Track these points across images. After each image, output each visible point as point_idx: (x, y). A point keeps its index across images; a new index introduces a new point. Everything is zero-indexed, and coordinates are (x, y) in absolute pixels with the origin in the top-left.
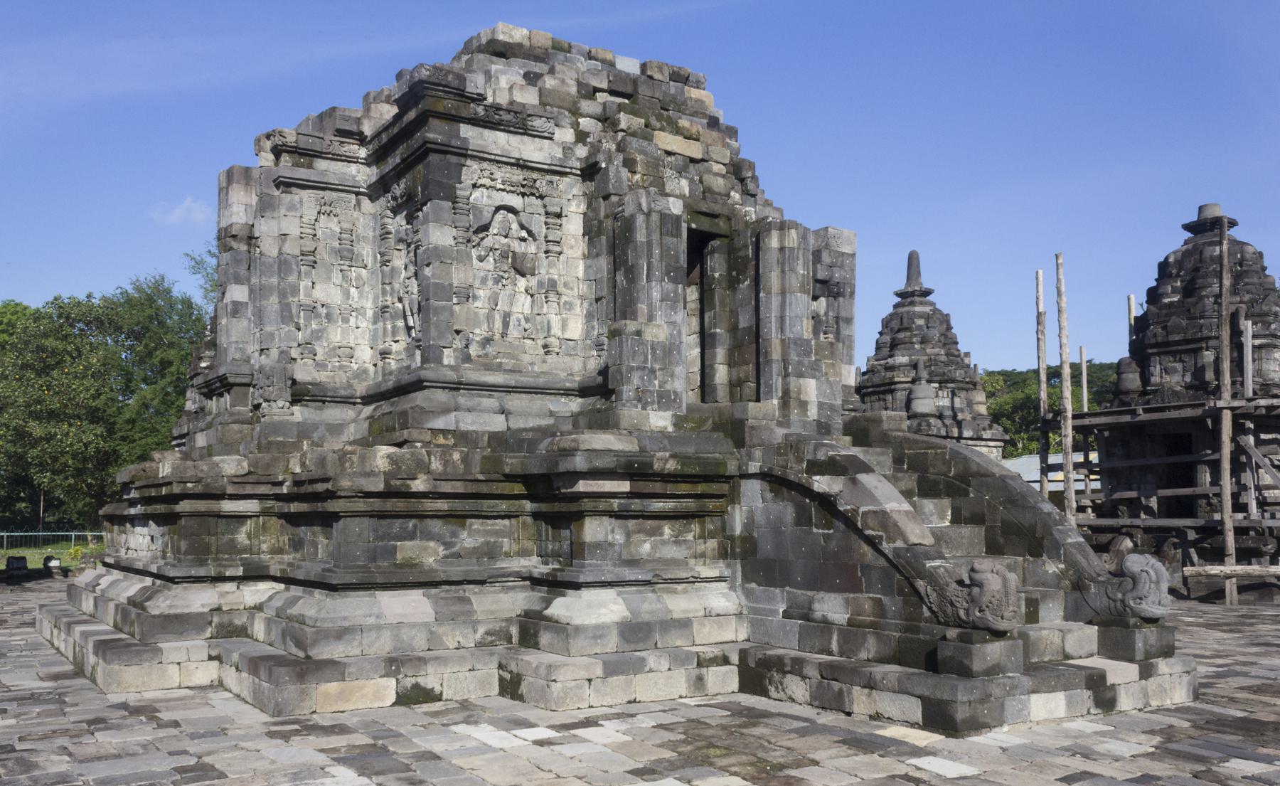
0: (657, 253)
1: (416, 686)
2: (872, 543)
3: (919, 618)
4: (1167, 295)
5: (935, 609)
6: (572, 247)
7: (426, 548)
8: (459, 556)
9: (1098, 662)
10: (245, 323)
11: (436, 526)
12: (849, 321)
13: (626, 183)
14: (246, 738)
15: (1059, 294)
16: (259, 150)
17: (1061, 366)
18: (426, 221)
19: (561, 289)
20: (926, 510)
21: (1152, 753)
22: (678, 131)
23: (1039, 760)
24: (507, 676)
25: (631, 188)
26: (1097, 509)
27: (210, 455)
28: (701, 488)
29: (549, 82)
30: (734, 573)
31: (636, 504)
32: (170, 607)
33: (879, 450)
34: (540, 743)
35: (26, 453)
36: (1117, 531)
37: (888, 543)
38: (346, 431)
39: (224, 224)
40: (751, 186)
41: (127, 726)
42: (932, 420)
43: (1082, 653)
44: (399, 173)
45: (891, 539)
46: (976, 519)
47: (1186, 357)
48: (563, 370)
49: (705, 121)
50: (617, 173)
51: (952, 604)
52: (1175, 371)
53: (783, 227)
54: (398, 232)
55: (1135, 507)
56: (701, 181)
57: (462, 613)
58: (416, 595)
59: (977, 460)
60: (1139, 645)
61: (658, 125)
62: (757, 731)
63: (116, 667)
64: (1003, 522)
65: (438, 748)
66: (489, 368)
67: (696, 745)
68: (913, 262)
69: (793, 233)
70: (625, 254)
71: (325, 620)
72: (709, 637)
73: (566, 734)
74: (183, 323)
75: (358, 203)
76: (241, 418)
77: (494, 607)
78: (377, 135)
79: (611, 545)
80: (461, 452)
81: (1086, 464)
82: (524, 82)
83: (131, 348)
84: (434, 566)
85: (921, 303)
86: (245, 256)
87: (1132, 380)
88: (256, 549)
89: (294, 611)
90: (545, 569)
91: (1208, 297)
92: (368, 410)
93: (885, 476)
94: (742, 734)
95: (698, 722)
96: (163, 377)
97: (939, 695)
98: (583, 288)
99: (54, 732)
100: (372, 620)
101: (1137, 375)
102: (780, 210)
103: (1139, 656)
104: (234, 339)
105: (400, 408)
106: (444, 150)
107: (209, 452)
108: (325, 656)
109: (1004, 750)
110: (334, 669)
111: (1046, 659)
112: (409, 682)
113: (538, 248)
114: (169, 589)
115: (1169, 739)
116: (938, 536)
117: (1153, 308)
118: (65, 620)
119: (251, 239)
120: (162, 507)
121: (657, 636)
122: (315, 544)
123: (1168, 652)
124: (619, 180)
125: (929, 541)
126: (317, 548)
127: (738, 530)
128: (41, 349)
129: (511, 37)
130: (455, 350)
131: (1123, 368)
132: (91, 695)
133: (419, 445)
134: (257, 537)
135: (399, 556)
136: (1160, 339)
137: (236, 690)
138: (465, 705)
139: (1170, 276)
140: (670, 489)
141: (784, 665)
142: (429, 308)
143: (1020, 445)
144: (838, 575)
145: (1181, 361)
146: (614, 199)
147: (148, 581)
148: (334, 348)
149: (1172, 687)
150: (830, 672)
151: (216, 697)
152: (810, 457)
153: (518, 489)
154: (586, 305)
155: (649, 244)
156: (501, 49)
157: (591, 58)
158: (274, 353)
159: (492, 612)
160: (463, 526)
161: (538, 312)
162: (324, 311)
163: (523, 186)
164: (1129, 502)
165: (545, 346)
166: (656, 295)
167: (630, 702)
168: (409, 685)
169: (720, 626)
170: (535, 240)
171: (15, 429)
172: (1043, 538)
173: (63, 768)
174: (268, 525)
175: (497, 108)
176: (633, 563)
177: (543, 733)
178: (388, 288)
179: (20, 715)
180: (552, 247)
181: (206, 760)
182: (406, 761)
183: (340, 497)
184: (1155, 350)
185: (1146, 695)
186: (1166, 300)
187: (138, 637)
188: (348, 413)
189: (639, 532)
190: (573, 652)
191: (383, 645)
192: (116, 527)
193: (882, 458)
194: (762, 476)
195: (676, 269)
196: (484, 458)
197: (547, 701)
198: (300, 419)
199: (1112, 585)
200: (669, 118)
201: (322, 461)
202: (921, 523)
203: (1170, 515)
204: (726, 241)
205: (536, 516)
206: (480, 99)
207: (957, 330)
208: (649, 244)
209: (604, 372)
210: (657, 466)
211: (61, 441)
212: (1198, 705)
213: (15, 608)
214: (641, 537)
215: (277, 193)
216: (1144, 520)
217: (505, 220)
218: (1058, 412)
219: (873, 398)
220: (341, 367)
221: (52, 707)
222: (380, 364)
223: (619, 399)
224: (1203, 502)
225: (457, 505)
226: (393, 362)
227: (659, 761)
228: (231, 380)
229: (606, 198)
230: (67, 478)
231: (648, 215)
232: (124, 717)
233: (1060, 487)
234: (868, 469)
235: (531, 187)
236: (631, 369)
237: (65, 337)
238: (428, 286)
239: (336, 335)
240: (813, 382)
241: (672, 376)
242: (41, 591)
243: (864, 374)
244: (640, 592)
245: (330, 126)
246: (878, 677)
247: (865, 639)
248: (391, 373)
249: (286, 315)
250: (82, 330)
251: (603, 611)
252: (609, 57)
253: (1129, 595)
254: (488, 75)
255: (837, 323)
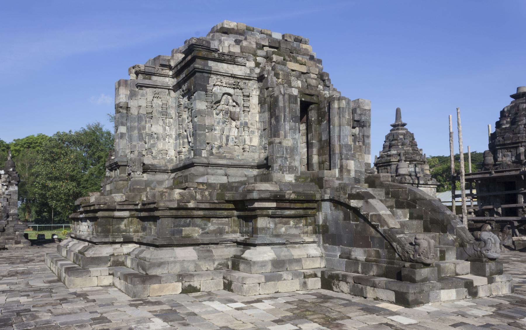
0: (288, 110)
1: (190, 286)
2: (375, 227)
3: (394, 258)
4: (504, 124)
5: (401, 255)
6: (254, 109)
7: (194, 230)
8: (208, 233)
9: (470, 277)
10: (125, 141)
11: (198, 221)
12: (368, 137)
13: (275, 83)
14: (121, 306)
15: (458, 124)
16: (130, 73)
17: (460, 155)
18: (195, 100)
19: (249, 125)
20: (399, 214)
21: (492, 315)
22: (297, 61)
23: (443, 317)
24: (226, 282)
25: (277, 85)
26: (477, 213)
27: (111, 194)
28: (305, 205)
29: (245, 43)
30: (319, 240)
31: (279, 212)
32: (94, 254)
33: (379, 189)
34: (238, 309)
35: (46, 193)
36: (484, 222)
37: (381, 227)
38: (164, 183)
39: (117, 102)
40: (327, 83)
41: (75, 302)
42: (407, 177)
43: (463, 273)
44: (184, 81)
45: (382, 226)
46: (419, 217)
47: (512, 150)
48: (251, 158)
49: (308, 57)
50: (271, 79)
51: (407, 252)
52: (508, 156)
53: (339, 99)
54: (184, 104)
55: (492, 212)
56: (306, 82)
57: (209, 256)
58: (190, 249)
59: (420, 193)
60: (488, 270)
61: (289, 59)
62: (327, 305)
63: (73, 278)
64: (430, 218)
65: (196, 311)
66: (221, 157)
67: (300, 311)
68: (398, 112)
69: (344, 102)
70: (275, 111)
71: (154, 259)
72: (309, 266)
73: (249, 305)
74: (107, 141)
75: (169, 93)
76: (123, 179)
77: (222, 254)
78: (176, 66)
79: (269, 228)
80: (209, 191)
81: (471, 194)
82: (234, 44)
83: (86, 151)
84: (198, 237)
85: (402, 129)
86: (125, 115)
87: (490, 160)
88: (128, 231)
89: (142, 256)
90: (242, 238)
91: (521, 125)
92: (173, 175)
93: (381, 201)
94: (321, 306)
95: (303, 301)
96: (99, 163)
97: (402, 290)
98: (259, 125)
99: (46, 304)
100: (172, 259)
101: (492, 158)
102: (339, 92)
103: (488, 274)
104: (121, 147)
105: (185, 174)
106: (202, 71)
107: (111, 192)
108: (154, 273)
109: (429, 313)
110: (157, 279)
111: (448, 275)
112: (187, 284)
113: (240, 109)
114: (94, 247)
115: (499, 309)
116: (403, 225)
117: (498, 130)
118: (55, 259)
119: (128, 108)
120: (92, 214)
121: (287, 266)
122: (151, 229)
123: (500, 272)
124: (272, 82)
125: (398, 226)
126: (151, 230)
127: (321, 222)
128: (53, 153)
129: (230, 26)
130: (207, 151)
131: (486, 155)
132: (63, 289)
133: (192, 189)
134: (129, 226)
135: (183, 233)
136: (501, 143)
137: (119, 287)
138: (209, 293)
139: (505, 116)
140: (292, 206)
141: (339, 278)
142: (197, 134)
143: (446, 187)
144: (361, 240)
145: (510, 151)
146: (270, 89)
147: (87, 244)
148: (160, 151)
149: (502, 287)
150: (357, 280)
151: (111, 290)
152: (349, 192)
153: (231, 206)
154: (260, 132)
155: (284, 107)
156: (226, 31)
157: (262, 33)
158: (136, 153)
159: (221, 256)
160: (209, 221)
161: (240, 134)
162: (156, 136)
163: (234, 85)
164: (490, 210)
165: (243, 149)
166: (287, 127)
167: (276, 292)
168: (187, 285)
169: (314, 261)
170: (239, 106)
171: (42, 184)
172: (447, 225)
173: (48, 318)
174: (133, 221)
175: (223, 54)
176: (278, 236)
177: (239, 305)
178: (181, 126)
179: (35, 297)
180: (245, 109)
181: (104, 315)
182: (183, 316)
183: (160, 210)
184: (499, 147)
185: (491, 290)
186: (504, 127)
187: (81, 266)
188: (165, 176)
189: (280, 223)
190: (253, 272)
191: (177, 269)
192: (76, 222)
193: (380, 193)
194: (330, 200)
195: (296, 117)
196: (218, 194)
197: (242, 292)
198: (146, 179)
199: (476, 244)
200: (293, 56)
201: (154, 196)
202: (395, 219)
203: (507, 215)
204: (317, 105)
205: (239, 217)
206: (216, 51)
207: (417, 140)
208: (284, 107)
209: (267, 159)
210: (287, 197)
211: (60, 189)
212: (513, 295)
213: (39, 254)
214: (281, 225)
215: (137, 90)
216: (496, 217)
217: (227, 98)
218: (458, 172)
219: (382, 168)
220: (163, 158)
221: (47, 294)
222: (178, 156)
223: (272, 170)
224: (521, 210)
225: (207, 213)
226: (183, 156)
227: (285, 317)
228: (119, 164)
229: (267, 89)
230: (62, 203)
231: (284, 95)
232: (74, 298)
233: (459, 204)
234: (373, 197)
235: (237, 85)
236: (277, 157)
237: (61, 148)
238: (196, 125)
239: (160, 145)
240: (352, 162)
241: (294, 160)
242: (49, 248)
243: (378, 158)
244: (280, 248)
245: (158, 63)
246: (377, 283)
247: (372, 267)
248: (182, 160)
249: (141, 138)
250: (67, 145)
251: (265, 255)
252: (269, 32)
253: (483, 249)
254: (220, 41)
255: (363, 138)
